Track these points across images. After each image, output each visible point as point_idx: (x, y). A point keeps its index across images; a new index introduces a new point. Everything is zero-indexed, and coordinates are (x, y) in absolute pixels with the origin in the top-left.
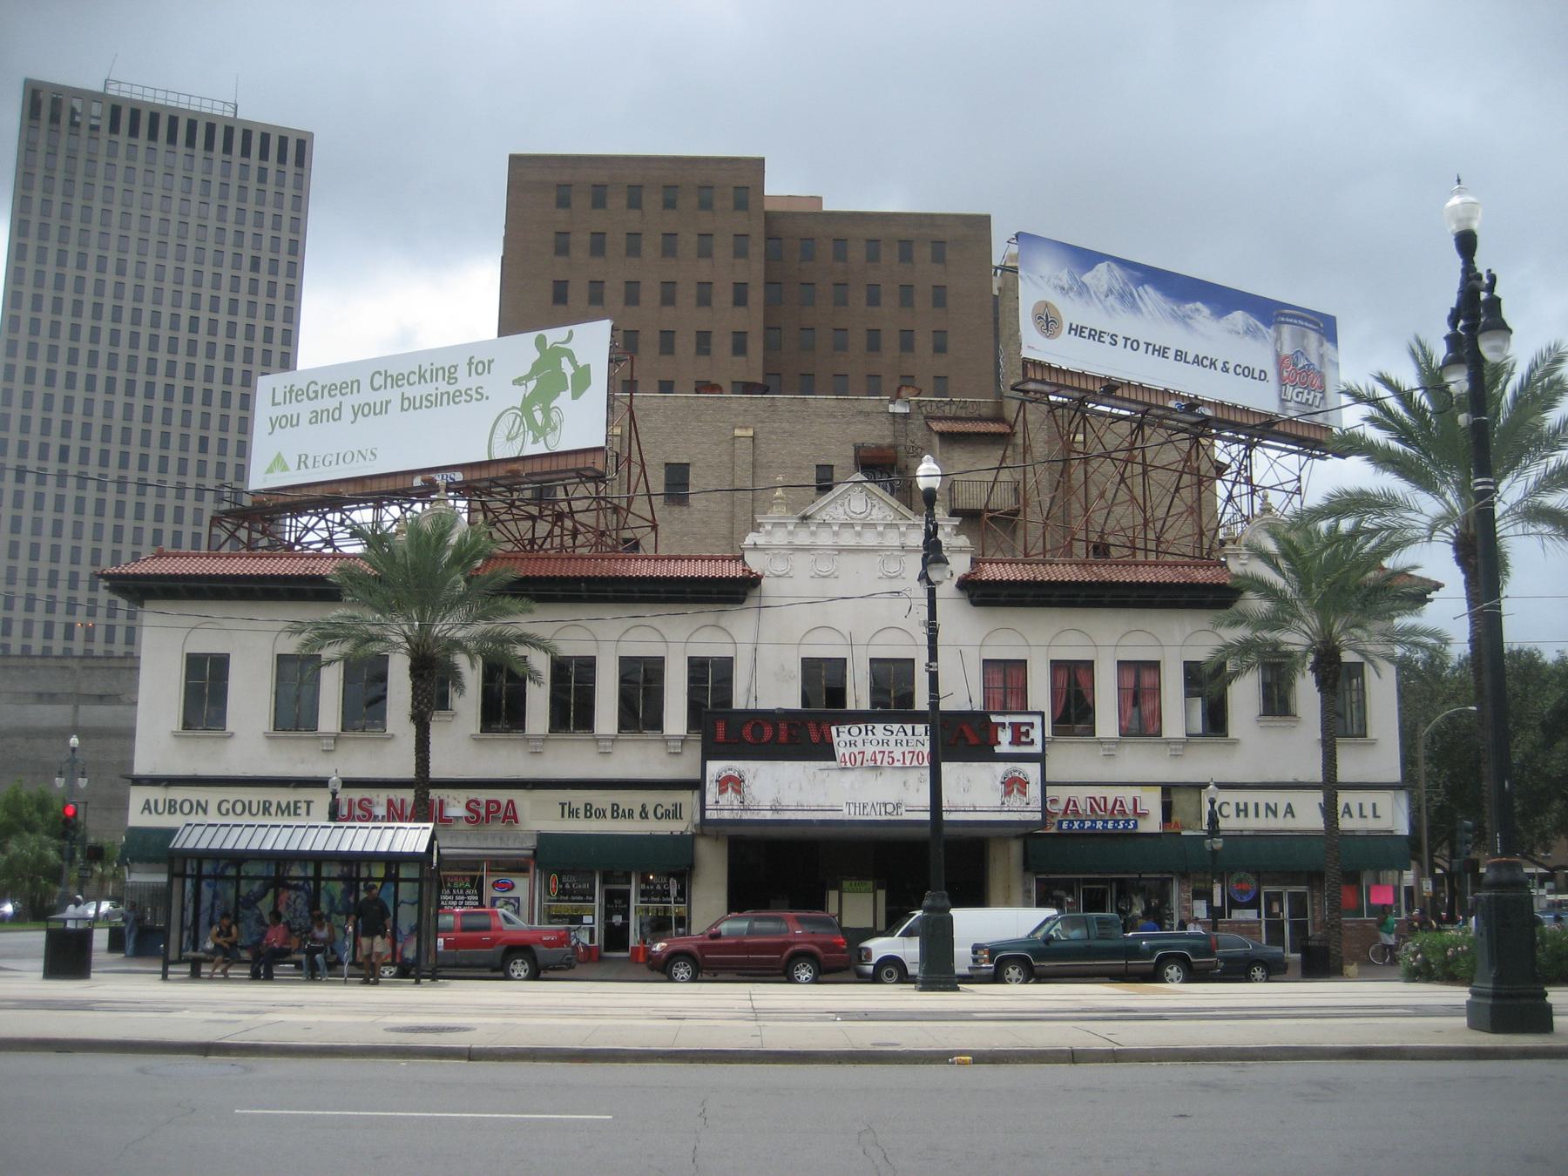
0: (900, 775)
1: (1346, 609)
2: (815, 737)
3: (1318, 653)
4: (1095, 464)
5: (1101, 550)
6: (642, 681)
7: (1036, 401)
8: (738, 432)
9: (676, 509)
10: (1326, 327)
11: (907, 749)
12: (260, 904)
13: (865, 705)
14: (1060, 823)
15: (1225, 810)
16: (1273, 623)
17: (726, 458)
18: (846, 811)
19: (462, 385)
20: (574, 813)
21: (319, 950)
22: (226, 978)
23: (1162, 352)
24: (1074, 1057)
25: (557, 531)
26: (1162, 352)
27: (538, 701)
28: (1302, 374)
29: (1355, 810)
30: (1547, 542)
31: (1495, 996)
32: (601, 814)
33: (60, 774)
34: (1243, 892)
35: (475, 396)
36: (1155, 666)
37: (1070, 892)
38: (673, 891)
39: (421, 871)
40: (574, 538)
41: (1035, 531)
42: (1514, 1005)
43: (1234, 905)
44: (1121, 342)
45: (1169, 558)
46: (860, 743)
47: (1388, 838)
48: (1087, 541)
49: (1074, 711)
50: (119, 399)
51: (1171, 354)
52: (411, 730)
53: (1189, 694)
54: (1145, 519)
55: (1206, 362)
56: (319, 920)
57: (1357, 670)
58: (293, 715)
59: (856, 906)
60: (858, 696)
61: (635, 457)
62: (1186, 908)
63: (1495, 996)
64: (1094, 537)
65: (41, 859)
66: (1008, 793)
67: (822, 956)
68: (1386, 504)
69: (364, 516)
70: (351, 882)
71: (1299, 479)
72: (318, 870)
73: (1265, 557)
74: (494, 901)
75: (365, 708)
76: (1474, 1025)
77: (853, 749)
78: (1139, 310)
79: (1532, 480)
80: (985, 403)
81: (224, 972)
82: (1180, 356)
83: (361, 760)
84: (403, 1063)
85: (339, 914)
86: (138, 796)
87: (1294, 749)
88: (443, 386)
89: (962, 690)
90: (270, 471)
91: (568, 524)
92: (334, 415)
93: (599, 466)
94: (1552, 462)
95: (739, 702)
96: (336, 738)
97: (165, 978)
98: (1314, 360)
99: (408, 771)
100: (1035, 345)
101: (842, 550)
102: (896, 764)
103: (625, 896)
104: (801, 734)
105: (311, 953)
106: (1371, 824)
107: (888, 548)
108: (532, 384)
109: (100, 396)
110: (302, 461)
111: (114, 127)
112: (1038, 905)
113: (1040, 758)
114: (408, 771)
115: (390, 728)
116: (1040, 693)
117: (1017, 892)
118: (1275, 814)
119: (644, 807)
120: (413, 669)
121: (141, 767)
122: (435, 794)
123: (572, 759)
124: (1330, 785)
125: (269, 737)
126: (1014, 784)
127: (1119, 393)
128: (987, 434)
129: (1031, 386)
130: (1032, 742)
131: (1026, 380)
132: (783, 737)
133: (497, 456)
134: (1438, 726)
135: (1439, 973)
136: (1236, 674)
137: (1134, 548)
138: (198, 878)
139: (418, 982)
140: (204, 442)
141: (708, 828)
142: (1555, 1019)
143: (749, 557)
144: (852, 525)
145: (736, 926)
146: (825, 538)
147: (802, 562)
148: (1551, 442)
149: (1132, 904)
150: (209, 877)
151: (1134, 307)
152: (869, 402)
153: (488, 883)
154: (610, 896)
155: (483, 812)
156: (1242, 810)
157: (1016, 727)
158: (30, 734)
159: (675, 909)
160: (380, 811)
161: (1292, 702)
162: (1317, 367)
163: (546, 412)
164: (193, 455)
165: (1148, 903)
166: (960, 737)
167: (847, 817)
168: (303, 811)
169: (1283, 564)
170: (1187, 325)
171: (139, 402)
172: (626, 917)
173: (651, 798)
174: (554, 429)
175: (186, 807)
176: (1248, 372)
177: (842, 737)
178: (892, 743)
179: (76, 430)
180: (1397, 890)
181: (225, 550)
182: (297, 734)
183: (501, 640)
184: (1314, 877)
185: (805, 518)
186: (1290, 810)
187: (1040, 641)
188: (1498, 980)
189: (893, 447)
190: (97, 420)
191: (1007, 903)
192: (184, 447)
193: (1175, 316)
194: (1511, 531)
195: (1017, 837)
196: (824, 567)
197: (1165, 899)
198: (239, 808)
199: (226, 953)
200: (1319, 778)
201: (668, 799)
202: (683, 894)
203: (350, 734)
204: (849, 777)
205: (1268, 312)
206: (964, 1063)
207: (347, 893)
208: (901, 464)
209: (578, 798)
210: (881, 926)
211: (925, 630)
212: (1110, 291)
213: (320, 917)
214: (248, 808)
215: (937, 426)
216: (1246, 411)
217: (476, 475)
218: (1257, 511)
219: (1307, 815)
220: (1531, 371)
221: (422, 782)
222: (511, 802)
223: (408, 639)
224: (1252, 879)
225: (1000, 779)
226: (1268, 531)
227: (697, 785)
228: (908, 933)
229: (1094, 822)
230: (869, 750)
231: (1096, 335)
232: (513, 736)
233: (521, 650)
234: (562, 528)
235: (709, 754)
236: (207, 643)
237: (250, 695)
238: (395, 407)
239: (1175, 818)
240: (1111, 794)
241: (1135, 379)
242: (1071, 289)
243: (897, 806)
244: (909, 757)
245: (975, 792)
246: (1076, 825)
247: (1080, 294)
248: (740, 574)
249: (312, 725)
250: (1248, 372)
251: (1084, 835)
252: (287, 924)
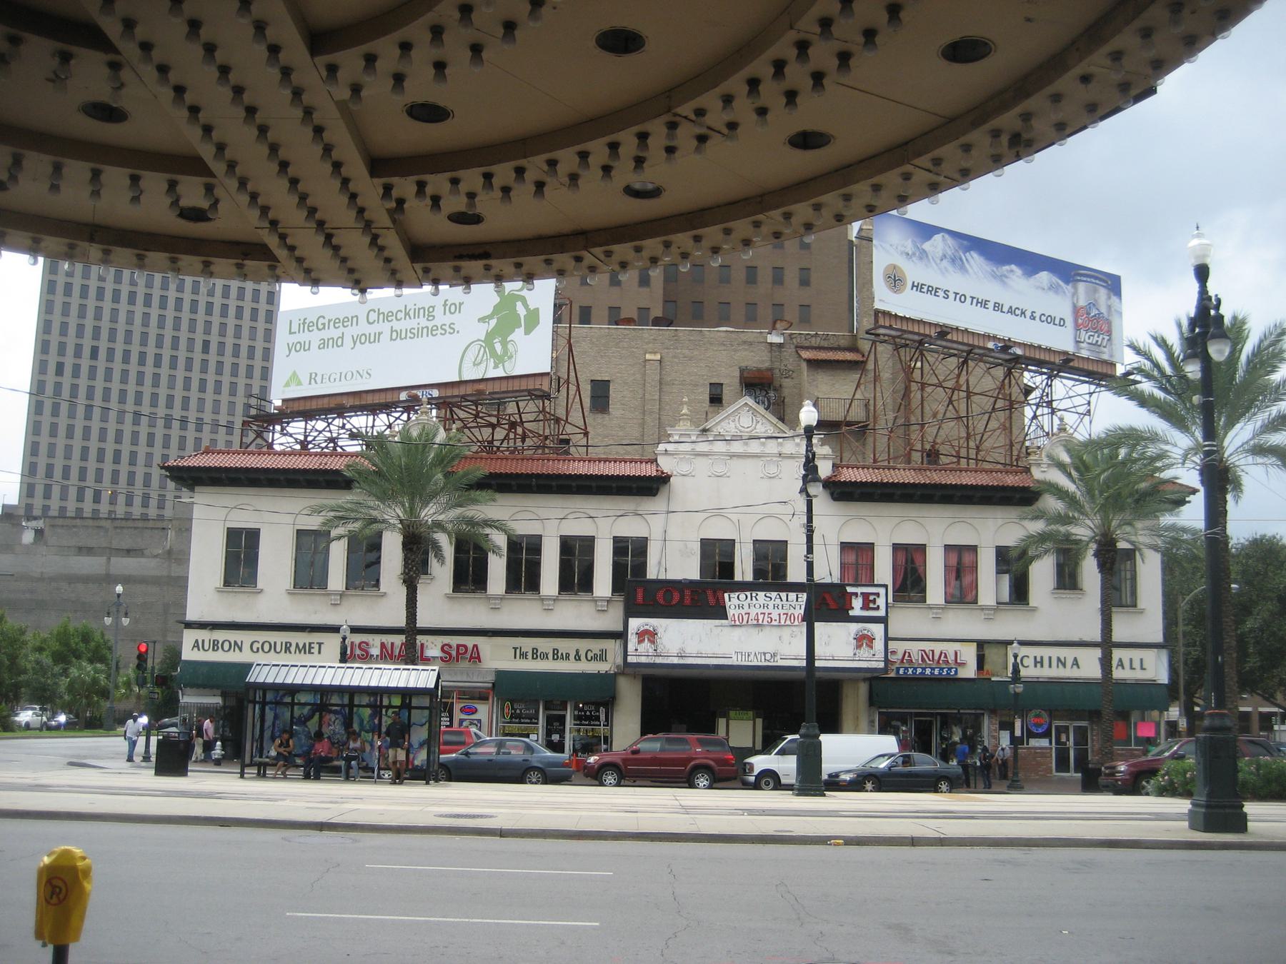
0: (776, 632)
1: (1122, 509)
2: (712, 601)
3: (1099, 543)
4: (929, 389)
5: (932, 456)
6: (576, 558)
7: (885, 341)
8: (648, 356)
9: (600, 416)
10: (1113, 284)
11: (782, 612)
12: (309, 724)
13: (749, 577)
14: (898, 669)
15: (1026, 662)
16: (1065, 520)
17: (638, 376)
18: (735, 658)
19: (437, 322)
20: (524, 656)
21: (354, 758)
22: (285, 778)
23: (983, 304)
24: (913, 842)
25: (512, 436)
26: (983, 304)
27: (497, 568)
28: (1095, 322)
29: (1127, 664)
30: (1271, 469)
31: (1207, 807)
32: (545, 656)
33: (109, 615)
34: (1038, 725)
35: (447, 328)
36: (973, 549)
37: (905, 723)
38: (603, 717)
39: (431, 701)
40: (523, 441)
41: (882, 443)
42: (1221, 814)
43: (1031, 735)
44: (952, 296)
45: (987, 466)
46: (746, 607)
47: (1152, 685)
48: (923, 451)
49: (910, 582)
50: (139, 309)
51: (991, 305)
52: (403, 591)
53: (999, 572)
54: (968, 434)
55: (1018, 312)
56: (353, 735)
57: (1130, 555)
58: (309, 575)
59: (740, 731)
60: (744, 569)
61: (572, 379)
62: (994, 737)
63: (1207, 807)
64: (928, 447)
65: (95, 681)
66: (859, 647)
67: (717, 768)
68: (1154, 438)
69: (360, 422)
70: (377, 709)
71: (1089, 403)
72: (351, 699)
73: (1061, 466)
74: (461, 721)
75: (364, 570)
76: (1192, 827)
77: (741, 611)
78: (967, 271)
79: (1259, 424)
80: (841, 335)
81: (283, 773)
82: (998, 307)
83: (360, 612)
84: (457, 838)
85: (367, 732)
86: (189, 637)
87: (1079, 615)
88: (423, 322)
89: (828, 569)
90: (287, 385)
91: (519, 430)
92: (337, 342)
93: (546, 388)
94: (1274, 410)
95: (652, 574)
96: (342, 595)
97: (242, 777)
98: (1104, 310)
99: (400, 620)
100: (885, 299)
101: (733, 456)
103: (562, 719)
104: (701, 599)
105: (348, 760)
106: (1138, 675)
107: (768, 455)
108: (493, 322)
109: (123, 307)
110: (312, 378)
112: (880, 733)
113: (884, 620)
114: (400, 620)
115: (383, 587)
116: (884, 570)
117: (864, 723)
118: (1064, 665)
119: (577, 652)
120: (404, 545)
121: (191, 616)
122: (420, 639)
123: (523, 613)
124: (1107, 644)
125: (289, 593)
126: (863, 640)
127: (949, 337)
128: (845, 361)
129: (881, 331)
130: (878, 608)
131: (877, 326)
132: (687, 600)
133: (465, 378)
134: (1196, 595)
135: (1180, 790)
136: (1038, 557)
137: (959, 457)
138: (264, 704)
139: (427, 783)
140: (206, 345)
141: (628, 669)
142: (1249, 824)
143: (661, 460)
145: (653, 746)
147: (701, 463)
148: (1276, 393)
149: (952, 733)
150: (271, 703)
151: (963, 268)
152: (752, 333)
153: (457, 707)
154: (550, 720)
155: (454, 653)
156: (1038, 662)
157: (865, 596)
158: (72, 579)
159: (602, 730)
160: (375, 651)
161: (1079, 579)
162: (1106, 314)
163: (504, 344)
164: (198, 356)
165: (964, 733)
166: (826, 603)
167: (736, 663)
168: (315, 650)
169: (1074, 473)
170: (1004, 283)
171: (155, 312)
172: (562, 737)
173: (583, 645)
174: (510, 357)
175: (226, 646)
176: (1050, 320)
177: (733, 601)
178: (771, 607)
179: (105, 334)
180: (1158, 725)
181: (252, 448)
182: (311, 591)
183: (471, 522)
184: (1094, 715)
185: (705, 430)
186: (1076, 663)
187: (884, 529)
188: (1210, 795)
189: (770, 370)
190: (121, 327)
191: (856, 730)
192: (190, 349)
193: (994, 276)
194: (1242, 462)
195: (865, 680)
196: (720, 469)
197: (978, 728)
198: (266, 647)
199: (286, 759)
200: (1098, 638)
201: (596, 646)
202: (609, 721)
203: (352, 592)
204: (738, 632)
205: (1067, 272)
206: (838, 844)
207: (372, 716)
208: (776, 383)
209: (527, 644)
210: (759, 746)
211: (804, 530)
212: (944, 257)
213: (354, 733)
214: (273, 647)
215: (806, 354)
216: (1049, 350)
217: (449, 392)
218: (1055, 430)
219: (1089, 666)
220: (1261, 341)
221: (411, 630)
222: (475, 646)
223: (401, 521)
224: (1045, 715)
225: (853, 636)
226: (1065, 446)
227: (621, 636)
228: (782, 752)
229: (924, 669)
230: (753, 612)
231: (933, 291)
232: (477, 595)
233: (488, 531)
234: (516, 434)
235: (630, 612)
236: (243, 520)
237: (276, 560)
238: (385, 337)
239: (986, 667)
240: (938, 647)
241: (962, 325)
242: (914, 254)
243: (774, 655)
244: (783, 617)
245: (837, 646)
246: (910, 671)
247: (921, 258)
248: (654, 474)
249: (323, 584)
250: (1050, 320)
252: (329, 738)
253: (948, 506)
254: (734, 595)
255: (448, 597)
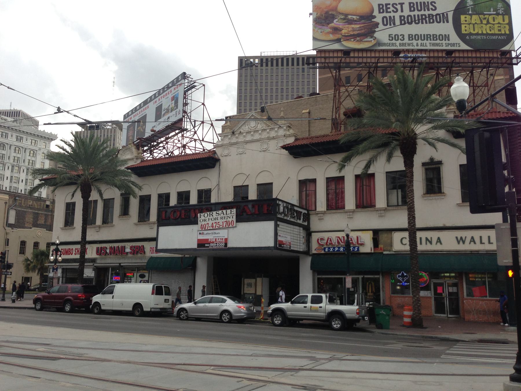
29: (477, 240)
99: (79, 238)
102: (221, 227)
111: (262, 66)
114: (79, 238)
118: (431, 243)
124: (412, 230)
144: (250, 132)
146: (241, 139)
156: (429, 241)
178: (219, 219)
186: (439, 240)
187: (321, 170)
229: (339, 248)
239: (381, 246)
251: (331, 254)
253: (310, 158)
254: (202, 214)
255: (62, 229)
